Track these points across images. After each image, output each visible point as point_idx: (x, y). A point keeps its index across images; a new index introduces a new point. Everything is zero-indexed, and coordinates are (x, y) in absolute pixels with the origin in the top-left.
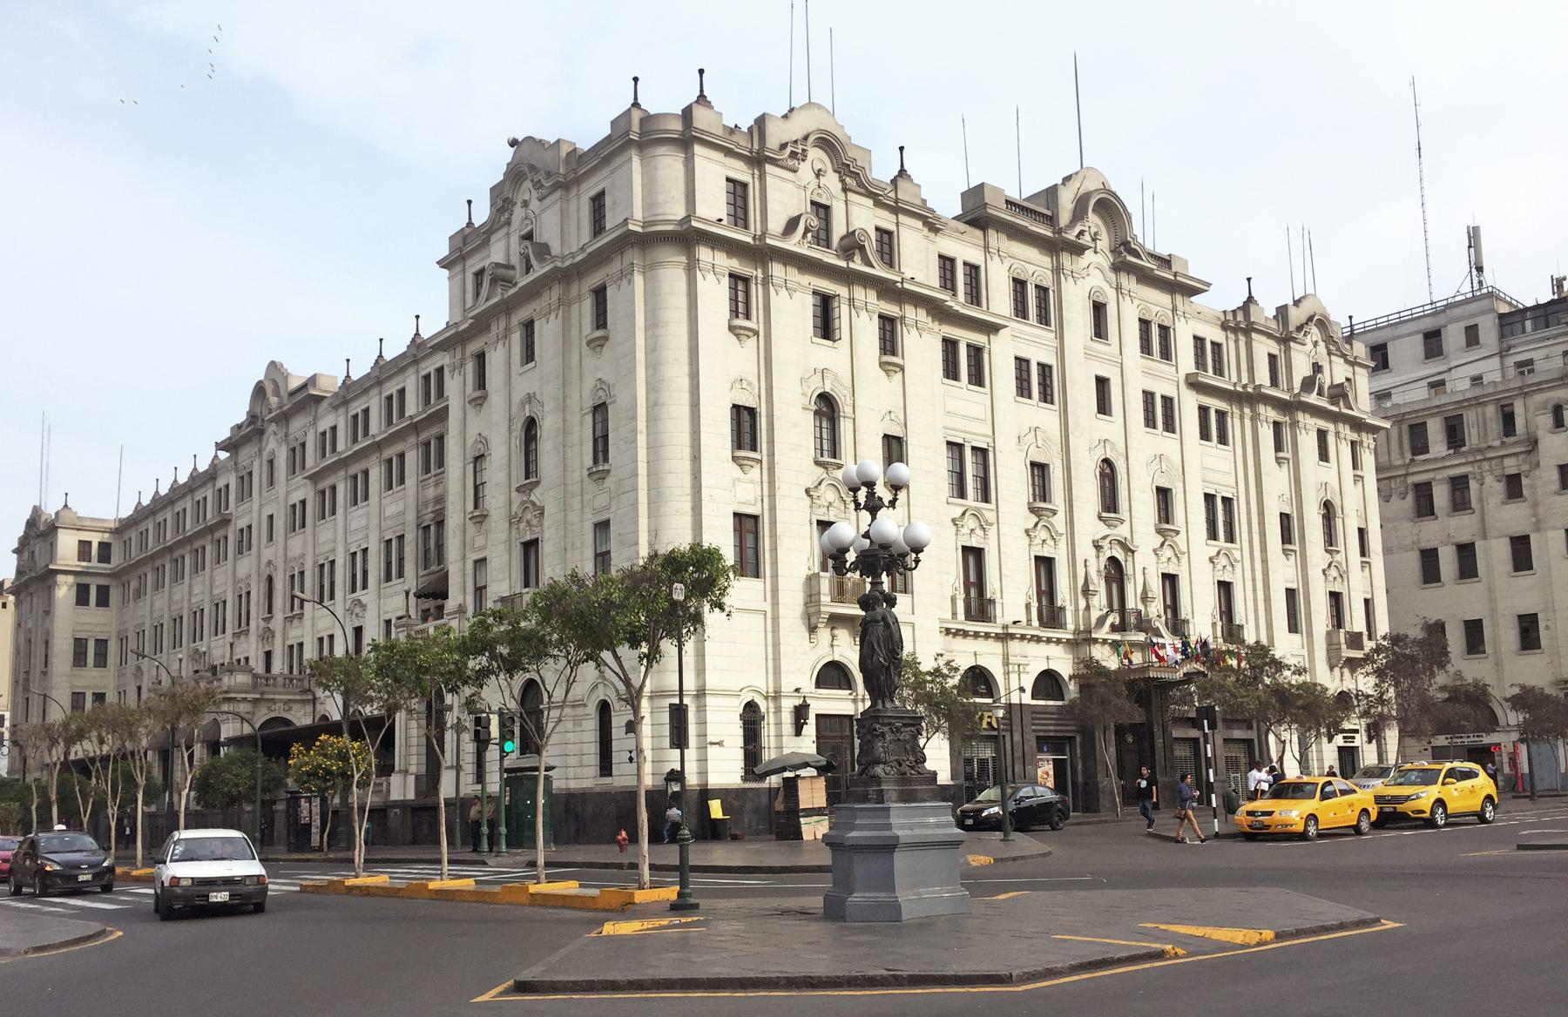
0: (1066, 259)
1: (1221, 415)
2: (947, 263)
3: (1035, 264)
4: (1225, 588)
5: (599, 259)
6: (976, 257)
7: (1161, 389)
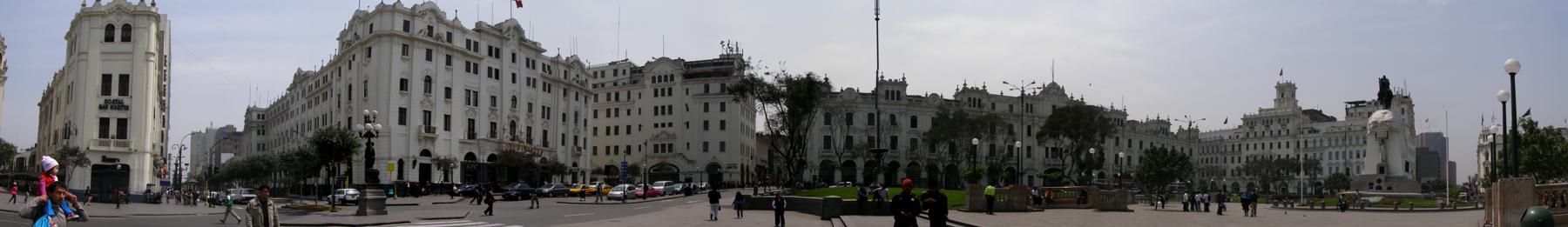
5: (369, 40)
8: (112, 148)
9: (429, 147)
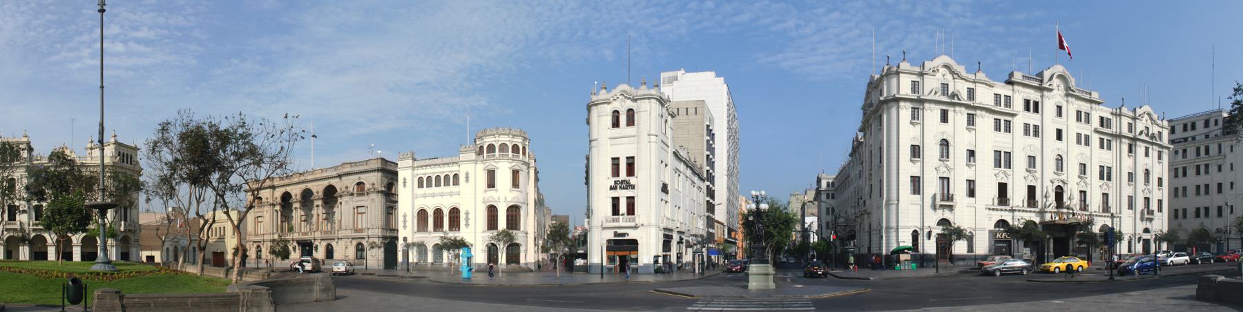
0: (1046, 93)
1: (1109, 141)
2: (997, 96)
3: (1034, 96)
4: (1105, 196)
6: (1009, 93)
7: (1084, 133)
8: (622, 224)
9: (947, 215)
